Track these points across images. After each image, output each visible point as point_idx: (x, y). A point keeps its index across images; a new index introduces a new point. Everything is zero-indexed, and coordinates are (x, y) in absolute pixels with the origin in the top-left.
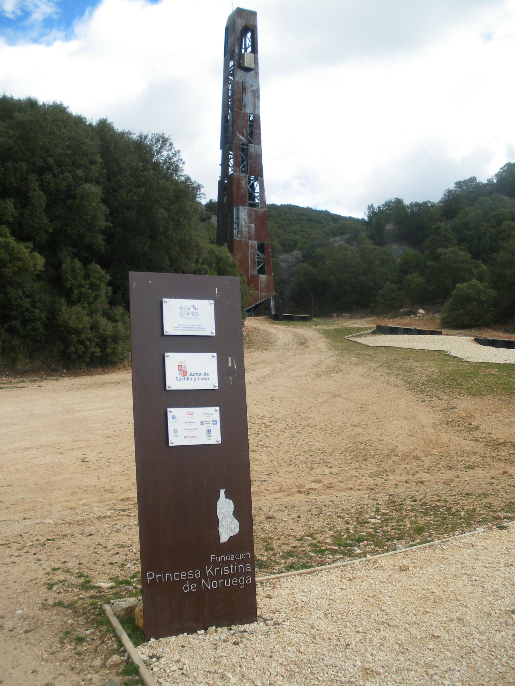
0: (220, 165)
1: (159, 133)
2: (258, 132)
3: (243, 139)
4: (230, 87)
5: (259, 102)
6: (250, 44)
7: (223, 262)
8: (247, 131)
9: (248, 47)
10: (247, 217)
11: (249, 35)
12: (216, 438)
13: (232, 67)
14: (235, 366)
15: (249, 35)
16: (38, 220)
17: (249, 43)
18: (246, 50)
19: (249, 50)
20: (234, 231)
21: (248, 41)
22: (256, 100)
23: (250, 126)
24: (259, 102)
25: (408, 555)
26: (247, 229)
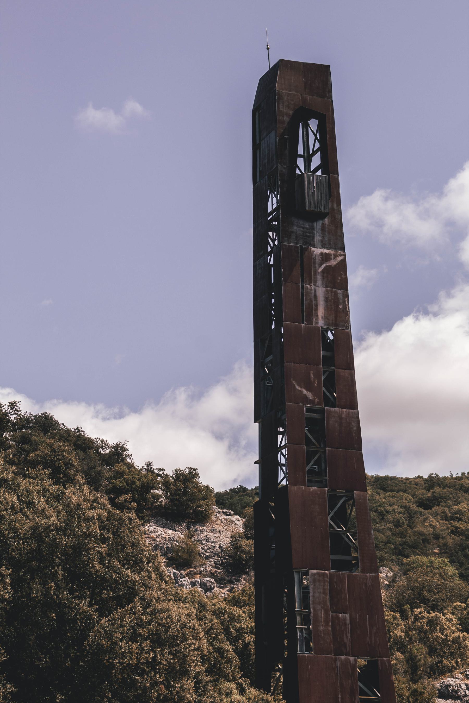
0: (256, 463)
1: (85, 432)
2: (343, 373)
3: (310, 395)
4: (271, 260)
5: (347, 296)
6: (317, 145)
7: (392, 546)
8: (318, 376)
9: (314, 153)
10: (328, 597)
11: (313, 124)
12: (298, 154)
13: (273, 211)
14: (282, 679)
15: (313, 124)
16: (411, 699)
17: (313, 144)
18: (308, 159)
19: (316, 161)
20: (299, 633)
21: (312, 138)
22: (340, 292)
23: (328, 361)
24: (346, 295)
25: (200, 603)
26: (330, 629)
